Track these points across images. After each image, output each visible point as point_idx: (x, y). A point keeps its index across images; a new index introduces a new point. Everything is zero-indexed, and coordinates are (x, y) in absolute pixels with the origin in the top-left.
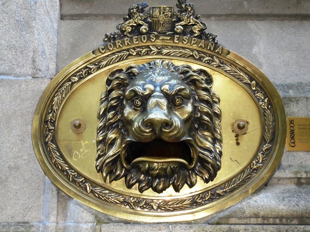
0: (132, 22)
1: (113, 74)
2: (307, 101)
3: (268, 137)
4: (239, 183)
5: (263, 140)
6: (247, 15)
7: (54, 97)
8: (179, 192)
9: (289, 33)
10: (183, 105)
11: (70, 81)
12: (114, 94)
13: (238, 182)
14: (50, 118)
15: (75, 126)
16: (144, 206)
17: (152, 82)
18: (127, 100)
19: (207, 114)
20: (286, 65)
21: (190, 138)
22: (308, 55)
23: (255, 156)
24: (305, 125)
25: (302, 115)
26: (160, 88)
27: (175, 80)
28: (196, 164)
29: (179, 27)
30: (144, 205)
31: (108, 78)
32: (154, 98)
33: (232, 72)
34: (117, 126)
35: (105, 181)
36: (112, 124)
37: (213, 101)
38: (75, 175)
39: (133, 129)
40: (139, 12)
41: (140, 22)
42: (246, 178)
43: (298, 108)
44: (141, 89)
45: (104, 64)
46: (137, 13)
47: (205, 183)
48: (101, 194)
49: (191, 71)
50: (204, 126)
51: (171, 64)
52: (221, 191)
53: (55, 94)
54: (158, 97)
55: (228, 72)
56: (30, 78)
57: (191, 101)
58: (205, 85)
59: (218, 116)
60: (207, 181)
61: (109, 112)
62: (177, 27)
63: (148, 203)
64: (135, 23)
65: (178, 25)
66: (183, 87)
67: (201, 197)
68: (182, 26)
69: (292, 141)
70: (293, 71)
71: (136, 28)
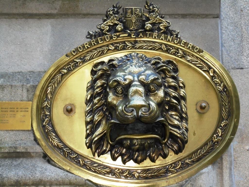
0: (110, 22)
1: (96, 66)
2: (11, 88)
3: (224, 114)
4: (203, 154)
5: (221, 119)
6: (90, 14)
7: (48, 87)
9: (15, 30)
10: (157, 92)
11: (60, 73)
12: (99, 83)
13: (203, 153)
14: (46, 105)
16: (128, 175)
17: (130, 73)
18: (110, 89)
19: (175, 98)
20: (9, 57)
22: (30, 48)
23: (215, 132)
25: (6, 99)
26: (138, 77)
27: (150, 71)
29: (148, 26)
30: (127, 174)
31: (92, 69)
32: (134, 87)
33: (193, 62)
34: (102, 109)
35: (94, 155)
36: (98, 108)
37: (180, 86)
38: (70, 152)
40: (115, 14)
41: (116, 22)
42: (209, 149)
43: (3, 94)
44: (122, 79)
45: (188, 59)
46: (113, 15)
47: (175, 154)
48: (92, 167)
49: (161, 63)
50: (173, 107)
51: (144, 57)
52: (190, 160)
53: (48, 85)
55: (190, 61)
57: (163, 88)
58: (173, 74)
59: (184, 98)
60: (176, 152)
61: (95, 98)
62: (146, 25)
63: (131, 173)
64: (112, 23)
65: (148, 24)
66: (156, 77)
67: (173, 167)
68: (150, 24)
70: (16, 62)
71: (113, 27)
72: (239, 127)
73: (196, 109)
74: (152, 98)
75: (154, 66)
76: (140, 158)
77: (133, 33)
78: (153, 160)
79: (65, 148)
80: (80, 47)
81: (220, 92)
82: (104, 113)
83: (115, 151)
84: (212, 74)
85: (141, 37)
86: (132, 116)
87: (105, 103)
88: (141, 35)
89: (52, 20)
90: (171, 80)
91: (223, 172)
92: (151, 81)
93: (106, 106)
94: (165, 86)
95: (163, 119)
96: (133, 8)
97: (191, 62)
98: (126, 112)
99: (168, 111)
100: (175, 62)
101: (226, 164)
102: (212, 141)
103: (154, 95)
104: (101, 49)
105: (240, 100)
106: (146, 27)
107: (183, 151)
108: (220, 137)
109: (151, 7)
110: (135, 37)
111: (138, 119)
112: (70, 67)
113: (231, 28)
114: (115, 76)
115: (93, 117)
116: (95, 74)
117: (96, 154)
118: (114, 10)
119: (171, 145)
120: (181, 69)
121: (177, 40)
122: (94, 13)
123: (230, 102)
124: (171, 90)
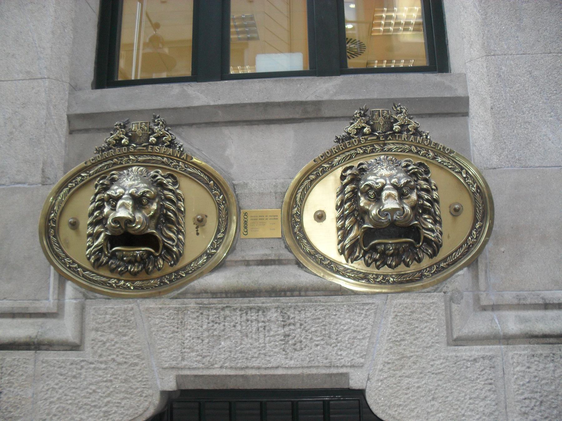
3: (479, 216)
5: (475, 221)
8: (409, 267)
12: (348, 188)
15: (198, 220)
17: (382, 177)
18: (362, 193)
19: (428, 200)
21: (154, 231)
23: (470, 234)
24: (257, 217)
26: (390, 181)
28: (422, 244)
29: (396, 127)
37: (432, 189)
39: (371, 217)
41: (363, 125)
50: (426, 211)
52: (445, 264)
54: (388, 189)
56: (40, 185)
57: (415, 191)
58: (424, 176)
60: (431, 256)
61: (346, 203)
69: (245, 230)
72: (494, 229)
73: (450, 212)
74: (405, 201)
75: (405, 169)
76: (394, 263)
77: (382, 136)
78: (407, 265)
79: (316, 254)
80: (327, 152)
81: (473, 193)
82: (356, 218)
83: (369, 257)
84: (465, 176)
85: (390, 139)
86: (386, 220)
87: (357, 208)
88: (390, 137)
89: (295, 126)
90: (422, 182)
91: (478, 275)
92: (404, 184)
93: (358, 211)
94: (417, 189)
95: (416, 222)
96: (381, 110)
97: (443, 164)
98: (381, 216)
99: (421, 215)
100: (426, 164)
101: (481, 266)
102: (467, 244)
103: (407, 198)
104: (349, 153)
105: (495, 202)
106: (394, 129)
107: (438, 255)
108: (475, 239)
109: (398, 108)
110: (384, 139)
111: (393, 223)
112: (318, 173)
113: (482, 127)
114: (366, 180)
115: (345, 222)
116: (345, 179)
117: (349, 260)
118: (360, 112)
119: (426, 249)
120: (432, 169)
121: (427, 141)
122: (337, 116)
123: (484, 203)
124: (423, 193)
